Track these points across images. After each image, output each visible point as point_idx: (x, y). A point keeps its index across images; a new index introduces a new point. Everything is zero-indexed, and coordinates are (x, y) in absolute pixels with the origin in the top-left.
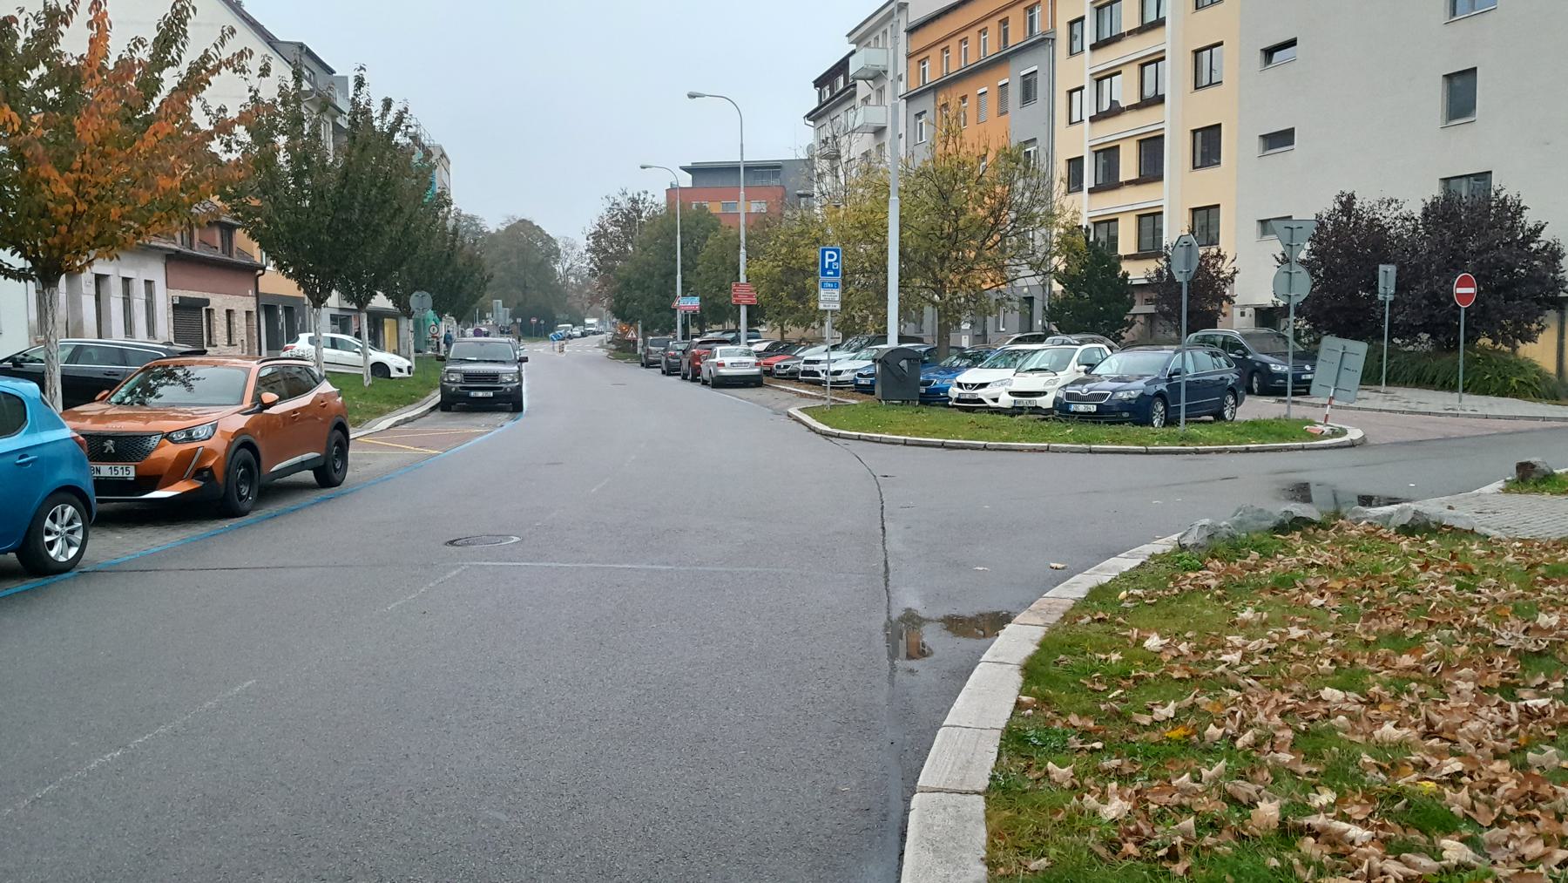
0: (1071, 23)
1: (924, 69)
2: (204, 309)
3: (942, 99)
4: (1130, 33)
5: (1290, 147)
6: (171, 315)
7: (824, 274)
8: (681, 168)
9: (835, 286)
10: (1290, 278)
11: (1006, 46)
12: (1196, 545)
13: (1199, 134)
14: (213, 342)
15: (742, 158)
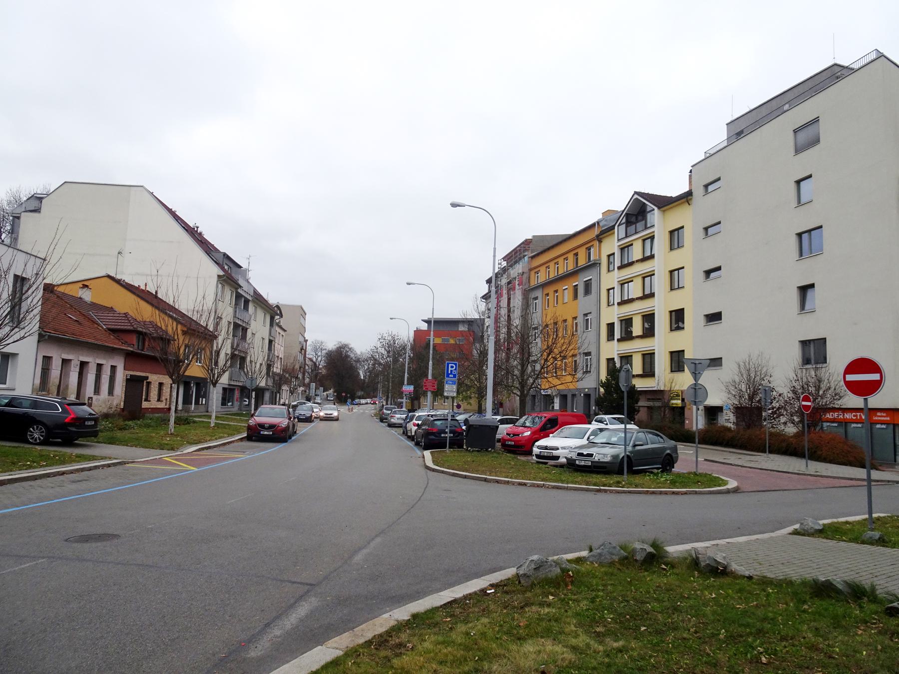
0: (609, 256)
1: (538, 276)
2: (145, 381)
3: (546, 292)
4: (637, 261)
5: (720, 322)
6: (125, 384)
7: (448, 376)
8: (422, 320)
9: (454, 383)
10: (695, 392)
11: (577, 267)
12: (525, 575)
13: (673, 313)
14: (149, 399)
15: (22, 274)
